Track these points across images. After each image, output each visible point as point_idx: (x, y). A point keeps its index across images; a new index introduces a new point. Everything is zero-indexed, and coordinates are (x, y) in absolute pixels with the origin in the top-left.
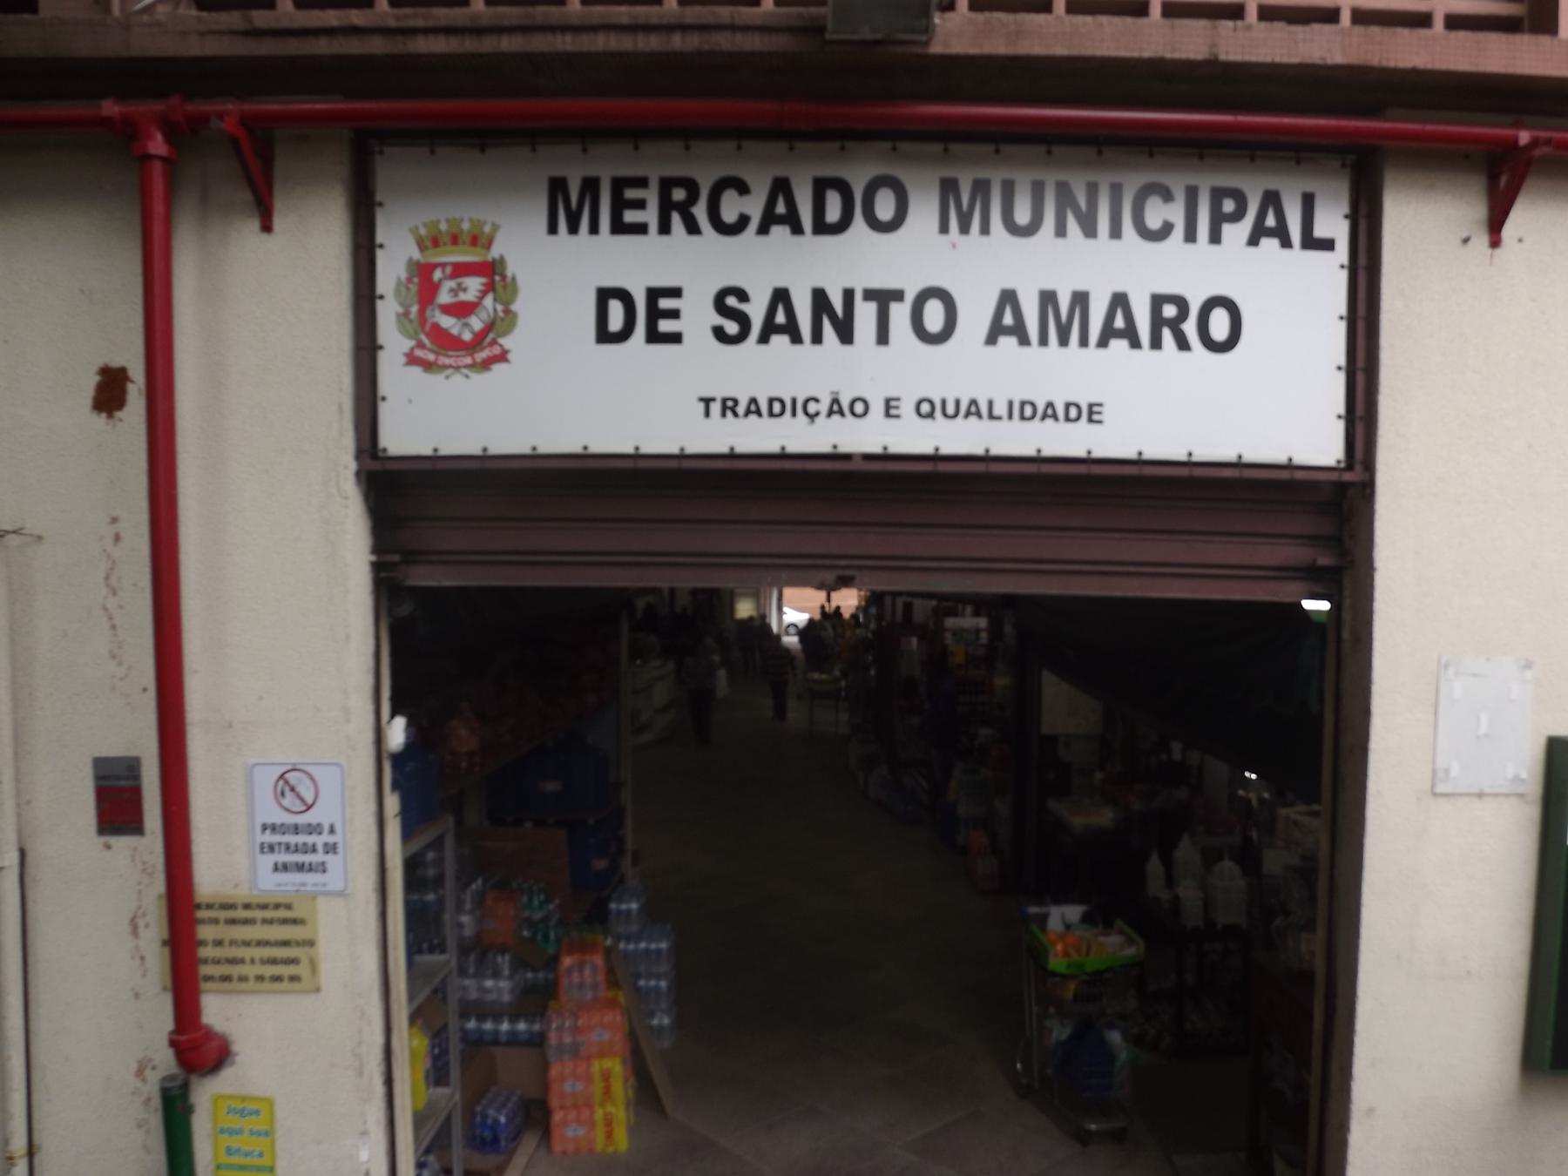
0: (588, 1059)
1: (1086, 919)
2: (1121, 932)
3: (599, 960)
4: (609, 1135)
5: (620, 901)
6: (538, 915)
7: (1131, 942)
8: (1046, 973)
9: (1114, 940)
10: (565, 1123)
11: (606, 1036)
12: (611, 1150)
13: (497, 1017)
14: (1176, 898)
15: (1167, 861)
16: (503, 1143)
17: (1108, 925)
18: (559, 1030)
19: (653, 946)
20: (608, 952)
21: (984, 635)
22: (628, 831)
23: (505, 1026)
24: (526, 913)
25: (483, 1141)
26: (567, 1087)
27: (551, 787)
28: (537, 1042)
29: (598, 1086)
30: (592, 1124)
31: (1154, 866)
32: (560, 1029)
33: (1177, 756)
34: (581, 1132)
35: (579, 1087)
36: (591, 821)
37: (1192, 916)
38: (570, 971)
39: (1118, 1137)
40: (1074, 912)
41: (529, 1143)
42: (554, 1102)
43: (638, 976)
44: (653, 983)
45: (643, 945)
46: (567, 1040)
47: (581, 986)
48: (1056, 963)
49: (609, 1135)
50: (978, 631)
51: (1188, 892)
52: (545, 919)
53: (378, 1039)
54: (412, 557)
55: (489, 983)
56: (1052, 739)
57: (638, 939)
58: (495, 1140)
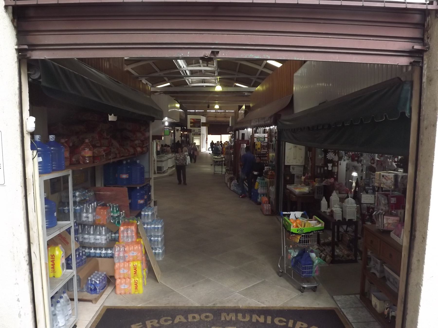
0: (129, 262)
1: (303, 216)
2: (316, 220)
3: (133, 228)
4: (136, 288)
5: (145, 212)
6: (116, 215)
7: (319, 222)
8: (290, 233)
9: (313, 222)
10: (121, 284)
11: (135, 254)
12: (137, 293)
13: (101, 248)
14: (332, 211)
15: (328, 200)
16: (98, 290)
17: (311, 218)
18: (118, 251)
19: (156, 226)
20: (137, 226)
21: (266, 139)
22: (152, 193)
23: (104, 252)
24: (112, 214)
25: (91, 290)
26: (121, 272)
27: (125, 176)
28: (112, 257)
29: (133, 271)
30: (130, 284)
31: (324, 202)
32: (119, 251)
33: (330, 168)
34: (126, 287)
35: (126, 271)
36: (138, 188)
37: (338, 217)
38: (123, 232)
39: (314, 289)
40: (299, 214)
41: (109, 290)
42: (117, 277)
43: (151, 236)
44: (156, 239)
45: (153, 226)
46: (121, 255)
47: (127, 237)
48: (293, 229)
49: (136, 288)
50: (265, 138)
51: (336, 209)
52: (118, 217)
53: (26, 247)
54: (33, 47)
55: (98, 237)
56: (289, 166)
57: (151, 224)
58: (95, 289)
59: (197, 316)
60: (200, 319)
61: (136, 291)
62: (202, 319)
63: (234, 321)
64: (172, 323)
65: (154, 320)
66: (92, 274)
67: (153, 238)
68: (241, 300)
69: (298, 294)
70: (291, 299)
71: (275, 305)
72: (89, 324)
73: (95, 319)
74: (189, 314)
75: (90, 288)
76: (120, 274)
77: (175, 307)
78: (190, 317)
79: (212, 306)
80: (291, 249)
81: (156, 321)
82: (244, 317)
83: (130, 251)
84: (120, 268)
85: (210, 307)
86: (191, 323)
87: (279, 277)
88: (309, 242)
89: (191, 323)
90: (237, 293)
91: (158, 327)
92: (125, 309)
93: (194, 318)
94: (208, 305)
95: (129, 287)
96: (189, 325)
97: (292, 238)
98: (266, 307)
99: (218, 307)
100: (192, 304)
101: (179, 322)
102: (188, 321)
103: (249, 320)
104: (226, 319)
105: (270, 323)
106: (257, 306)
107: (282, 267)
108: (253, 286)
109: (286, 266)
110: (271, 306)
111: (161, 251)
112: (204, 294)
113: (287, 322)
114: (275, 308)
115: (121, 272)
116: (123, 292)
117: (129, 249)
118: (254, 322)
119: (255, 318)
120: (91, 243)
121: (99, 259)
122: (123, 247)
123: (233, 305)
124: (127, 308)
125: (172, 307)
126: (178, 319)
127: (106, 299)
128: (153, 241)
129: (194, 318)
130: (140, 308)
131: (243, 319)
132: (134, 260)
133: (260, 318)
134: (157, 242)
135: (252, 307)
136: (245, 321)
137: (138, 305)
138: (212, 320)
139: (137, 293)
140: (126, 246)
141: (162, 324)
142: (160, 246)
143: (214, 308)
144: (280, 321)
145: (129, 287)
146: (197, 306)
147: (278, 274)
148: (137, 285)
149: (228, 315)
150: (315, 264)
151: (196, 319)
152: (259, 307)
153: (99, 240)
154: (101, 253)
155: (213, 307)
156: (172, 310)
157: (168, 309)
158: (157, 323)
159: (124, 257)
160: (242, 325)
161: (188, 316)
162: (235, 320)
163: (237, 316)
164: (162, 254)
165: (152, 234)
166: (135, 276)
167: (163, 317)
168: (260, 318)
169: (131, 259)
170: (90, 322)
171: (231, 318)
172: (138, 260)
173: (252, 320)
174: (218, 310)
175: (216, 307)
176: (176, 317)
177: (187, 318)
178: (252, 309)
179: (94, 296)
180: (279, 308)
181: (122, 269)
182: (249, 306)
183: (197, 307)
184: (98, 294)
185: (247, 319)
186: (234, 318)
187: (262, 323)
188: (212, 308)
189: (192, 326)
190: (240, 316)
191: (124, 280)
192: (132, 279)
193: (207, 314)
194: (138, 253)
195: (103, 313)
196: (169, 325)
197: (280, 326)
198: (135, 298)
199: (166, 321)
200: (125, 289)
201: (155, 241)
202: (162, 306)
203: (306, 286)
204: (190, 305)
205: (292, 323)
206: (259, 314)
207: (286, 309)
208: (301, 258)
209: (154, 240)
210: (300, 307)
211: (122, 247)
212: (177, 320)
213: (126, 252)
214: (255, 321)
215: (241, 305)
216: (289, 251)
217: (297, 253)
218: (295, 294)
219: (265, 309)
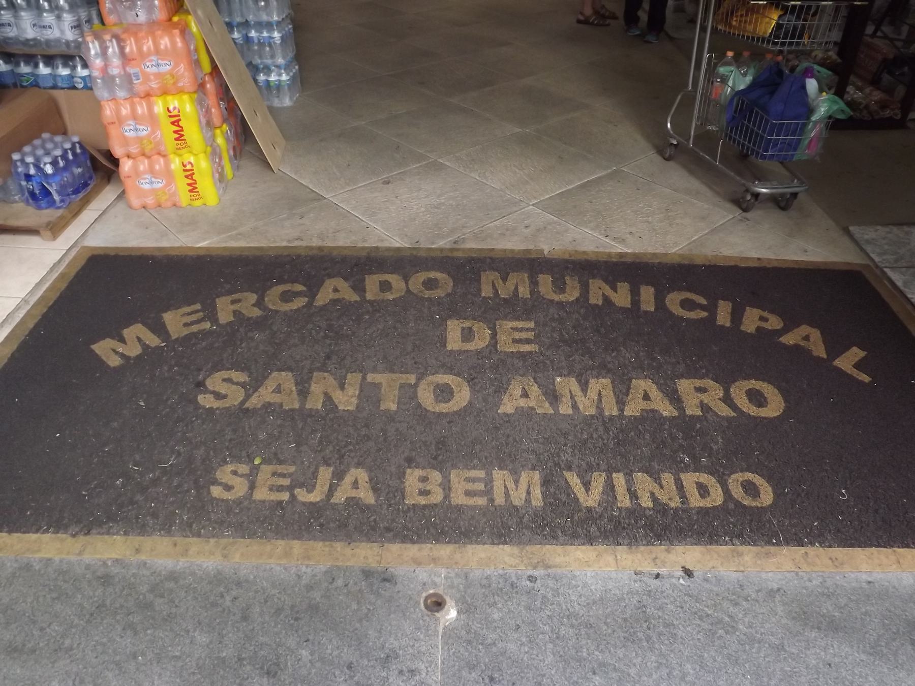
0: (148, 95)
10: (138, 174)
25: (32, 195)
29: (168, 130)
39: (782, 203)
59: (394, 279)
60: (408, 291)
61: (193, 197)
62: (415, 292)
63: (525, 300)
64: (309, 305)
65: (246, 294)
66: (28, 142)
67: (253, 32)
68: (545, 228)
69: (732, 216)
70: (714, 231)
71: (660, 250)
72: (18, 308)
73: (45, 291)
74: (370, 274)
75: (28, 189)
76: (126, 141)
77: (320, 249)
78: (372, 282)
79: (448, 247)
80: (728, 64)
81: (253, 297)
82: (560, 287)
83: (143, 56)
84: (120, 121)
85: (441, 250)
86: (375, 304)
87: (667, 162)
88: (801, 37)
89: (377, 307)
90: (531, 207)
91: (257, 317)
92: (153, 258)
93: (385, 286)
94: (433, 243)
95: (169, 184)
96: (368, 312)
97: (740, 21)
98: (634, 254)
99: (470, 250)
100: (382, 241)
101: (331, 300)
102: (365, 297)
103: (577, 299)
104: (497, 291)
105: (652, 309)
106: (601, 250)
107: (681, 129)
108: (583, 186)
109: (699, 123)
110: (650, 250)
111: (284, 77)
112: (423, 209)
113: (712, 309)
114: (664, 260)
115: (126, 134)
116: (150, 201)
117: (140, 49)
118: (597, 305)
119: (598, 290)
120: (28, 40)
121: (55, 93)
122: (114, 41)
123: (522, 247)
124: (157, 254)
125: (311, 248)
126: (330, 291)
127: (95, 225)
128: (256, 41)
129: (385, 286)
130: (202, 253)
131: (555, 292)
132: (165, 92)
133: (617, 292)
134: (270, 45)
135: (584, 252)
136: (564, 300)
137: (199, 242)
138: (448, 295)
139: (198, 203)
140: (123, 36)
141: (273, 308)
142: (280, 61)
143: (456, 254)
144: (687, 304)
145: (169, 184)
146: (398, 245)
147: (660, 152)
148: (194, 177)
149: (504, 279)
150: (814, 118)
151: (392, 293)
152: (609, 255)
153: (50, 27)
154: (73, 77)
155: (452, 250)
156: (312, 259)
157: (299, 256)
158: (254, 305)
159: (128, 79)
160: (556, 316)
161: (364, 280)
162: (529, 296)
163: (534, 283)
164: (289, 85)
165: (251, 18)
166: (179, 146)
167: (278, 283)
168: (617, 292)
169: (154, 85)
170: (25, 301)
171: (516, 289)
172: (180, 91)
173: (588, 300)
174: (471, 261)
175: (464, 250)
176: (323, 281)
177: (359, 288)
178: (587, 261)
179: (49, 214)
180: (677, 260)
181: (130, 125)
182: (576, 251)
183: (398, 249)
184: (59, 208)
185: (572, 294)
186: (524, 292)
187: (623, 310)
188: (450, 255)
189: (378, 315)
190: (545, 282)
191: (146, 161)
192: (172, 156)
193: (433, 275)
194: (177, 65)
195: (73, 274)
196: (298, 310)
197: (688, 320)
198: (190, 221)
199: (286, 297)
200: (154, 191)
201: (261, 44)
202: (278, 245)
203: (764, 190)
204: (371, 243)
205: (730, 311)
206: (610, 278)
207: (699, 262)
208: (772, 93)
209: (259, 41)
210: (747, 259)
211: (111, 41)
212: (325, 296)
213: (130, 60)
214: (600, 302)
215: (548, 246)
216: (722, 70)
217: (749, 79)
218: (726, 214)
219: (629, 260)
